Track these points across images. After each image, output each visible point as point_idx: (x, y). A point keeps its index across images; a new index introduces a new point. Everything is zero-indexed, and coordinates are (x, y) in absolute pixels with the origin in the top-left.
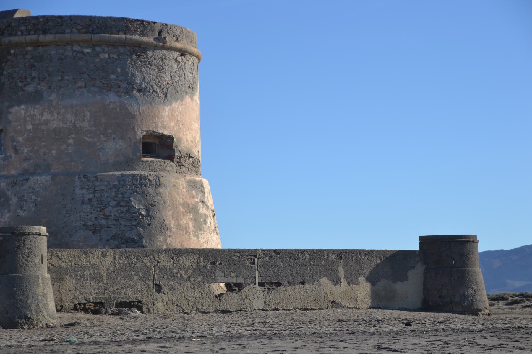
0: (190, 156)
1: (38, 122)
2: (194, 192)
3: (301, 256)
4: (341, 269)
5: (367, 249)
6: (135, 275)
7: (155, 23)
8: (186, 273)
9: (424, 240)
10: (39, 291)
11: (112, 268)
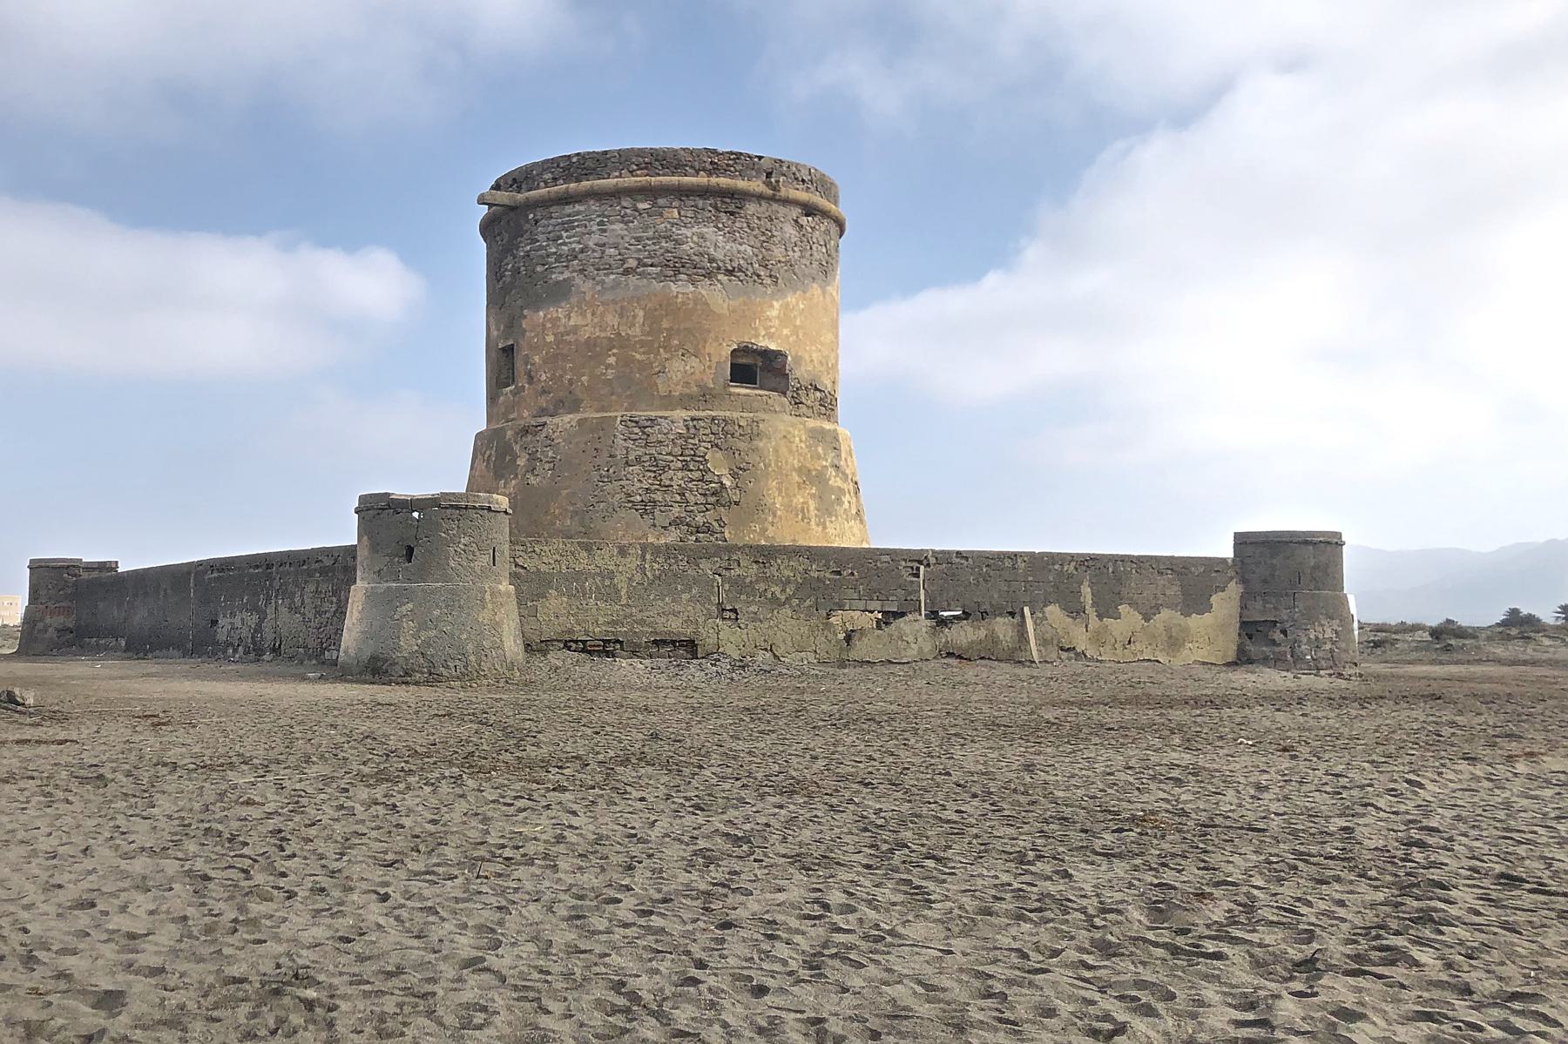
0: (816, 389)
1: (562, 329)
2: (820, 450)
3: (1008, 563)
4: (1086, 591)
5: (1136, 554)
6: (683, 592)
7: (760, 158)
8: (783, 591)
9: (1242, 540)
10: (359, 628)
11: (638, 577)
